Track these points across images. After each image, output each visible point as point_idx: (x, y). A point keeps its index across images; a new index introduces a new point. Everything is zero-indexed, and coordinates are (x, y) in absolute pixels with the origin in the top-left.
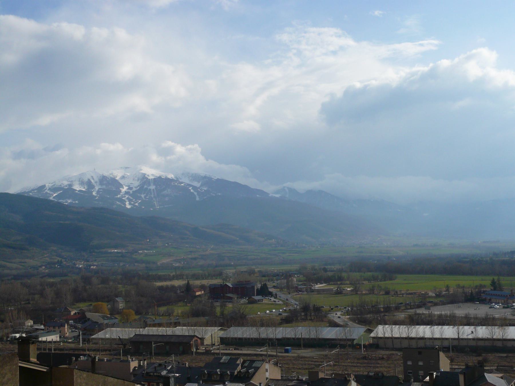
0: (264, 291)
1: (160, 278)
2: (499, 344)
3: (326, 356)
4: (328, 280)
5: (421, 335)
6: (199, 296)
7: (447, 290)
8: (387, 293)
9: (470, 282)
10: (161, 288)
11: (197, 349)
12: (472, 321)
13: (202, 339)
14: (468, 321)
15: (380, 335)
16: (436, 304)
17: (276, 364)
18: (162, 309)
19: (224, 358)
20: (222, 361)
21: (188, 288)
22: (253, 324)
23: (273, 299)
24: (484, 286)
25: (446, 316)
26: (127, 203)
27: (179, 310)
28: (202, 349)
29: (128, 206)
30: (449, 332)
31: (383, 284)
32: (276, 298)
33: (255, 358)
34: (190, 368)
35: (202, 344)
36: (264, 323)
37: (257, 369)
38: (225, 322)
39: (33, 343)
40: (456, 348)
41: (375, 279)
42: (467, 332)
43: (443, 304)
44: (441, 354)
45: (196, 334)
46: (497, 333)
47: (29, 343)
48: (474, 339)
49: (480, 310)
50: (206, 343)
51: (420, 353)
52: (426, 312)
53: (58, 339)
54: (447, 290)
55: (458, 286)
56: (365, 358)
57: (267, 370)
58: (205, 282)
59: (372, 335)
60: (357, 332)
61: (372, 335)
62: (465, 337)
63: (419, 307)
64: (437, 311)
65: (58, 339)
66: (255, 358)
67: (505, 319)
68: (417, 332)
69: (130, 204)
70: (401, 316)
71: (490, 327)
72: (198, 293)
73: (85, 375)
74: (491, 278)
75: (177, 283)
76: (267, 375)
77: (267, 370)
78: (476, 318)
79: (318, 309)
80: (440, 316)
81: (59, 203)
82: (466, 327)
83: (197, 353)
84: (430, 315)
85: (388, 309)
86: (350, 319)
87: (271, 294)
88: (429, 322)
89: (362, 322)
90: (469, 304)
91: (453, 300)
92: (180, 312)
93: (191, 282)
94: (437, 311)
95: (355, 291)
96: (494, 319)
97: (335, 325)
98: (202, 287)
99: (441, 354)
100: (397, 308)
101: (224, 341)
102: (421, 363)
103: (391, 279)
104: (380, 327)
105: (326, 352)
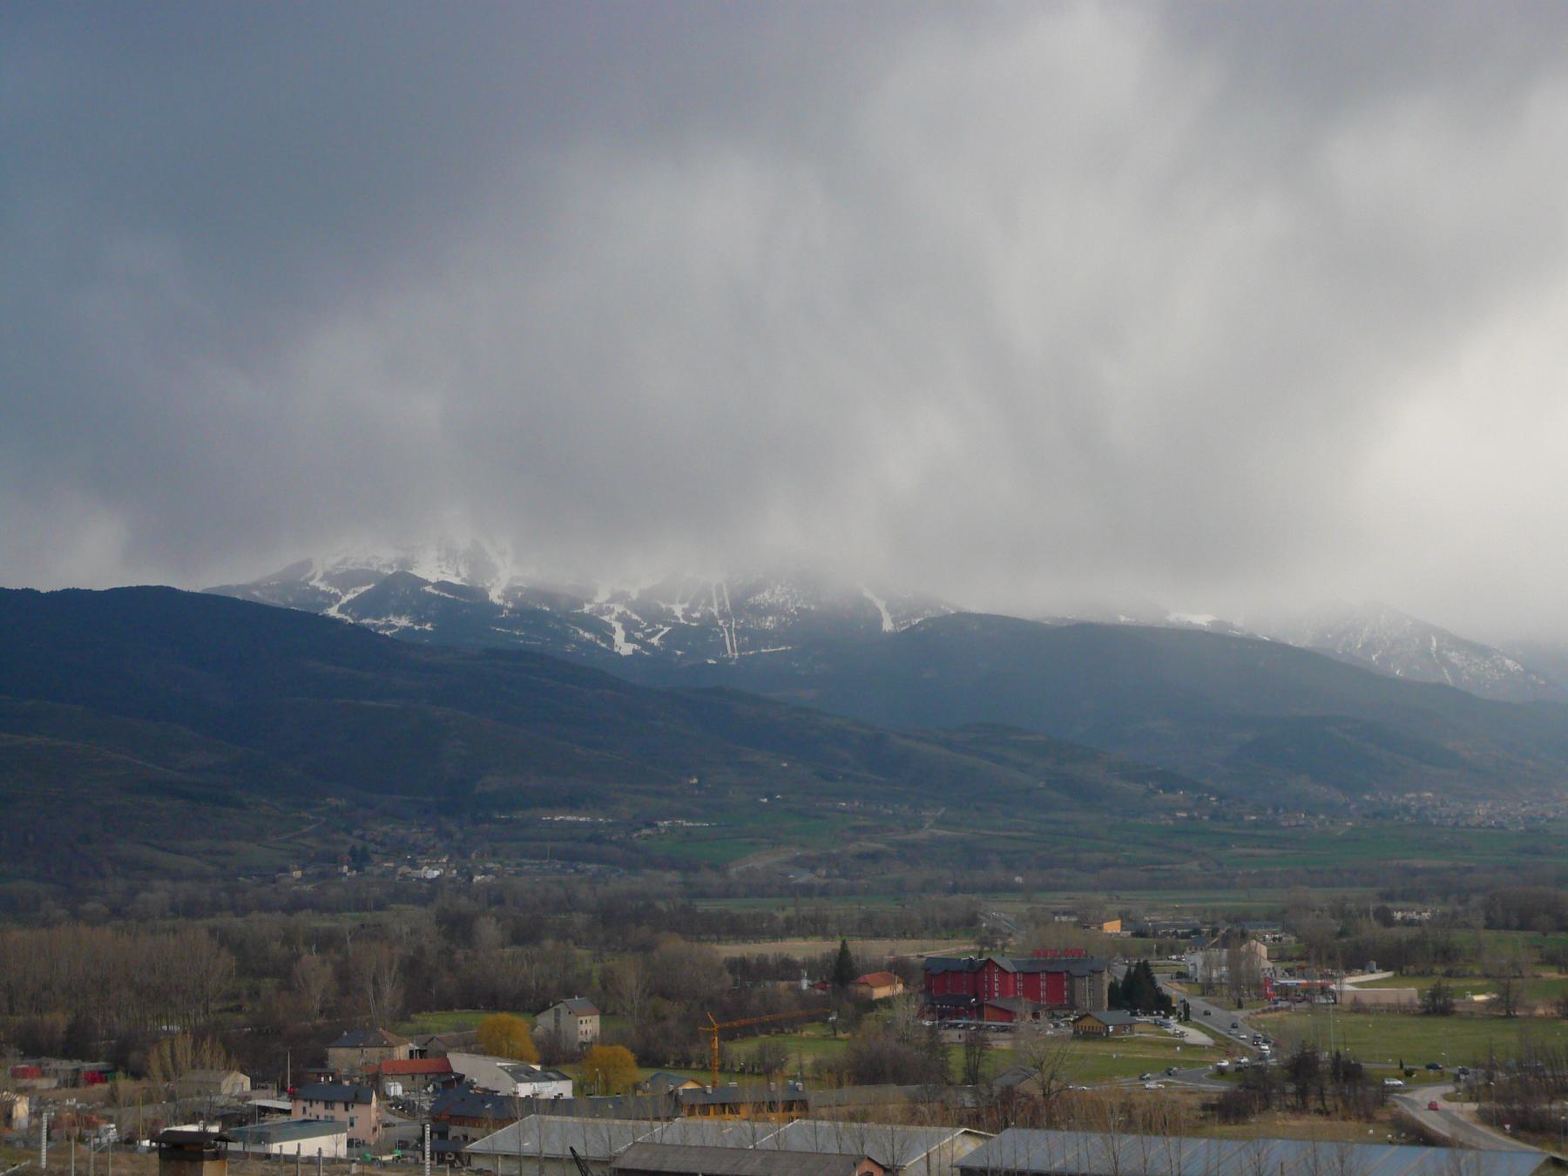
0: (1137, 994)
1: (737, 929)
4: (1396, 960)
6: (887, 1002)
10: (740, 967)
18: (742, 1050)
21: (842, 972)
22: (1091, 1117)
23: (1174, 1026)
26: (619, 636)
27: (805, 1051)
29: (625, 649)
32: (1185, 1018)
45: (869, 1150)
65: (342, 1151)
69: (629, 638)
72: (880, 993)
75: (800, 948)
79: (1348, 1072)
81: (365, 630)
86: (1486, 1118)
87: (1163, 1004)
92: (808, 1060)
93: (857, 946)
95: (1505, 1008)
98: (900, 969)
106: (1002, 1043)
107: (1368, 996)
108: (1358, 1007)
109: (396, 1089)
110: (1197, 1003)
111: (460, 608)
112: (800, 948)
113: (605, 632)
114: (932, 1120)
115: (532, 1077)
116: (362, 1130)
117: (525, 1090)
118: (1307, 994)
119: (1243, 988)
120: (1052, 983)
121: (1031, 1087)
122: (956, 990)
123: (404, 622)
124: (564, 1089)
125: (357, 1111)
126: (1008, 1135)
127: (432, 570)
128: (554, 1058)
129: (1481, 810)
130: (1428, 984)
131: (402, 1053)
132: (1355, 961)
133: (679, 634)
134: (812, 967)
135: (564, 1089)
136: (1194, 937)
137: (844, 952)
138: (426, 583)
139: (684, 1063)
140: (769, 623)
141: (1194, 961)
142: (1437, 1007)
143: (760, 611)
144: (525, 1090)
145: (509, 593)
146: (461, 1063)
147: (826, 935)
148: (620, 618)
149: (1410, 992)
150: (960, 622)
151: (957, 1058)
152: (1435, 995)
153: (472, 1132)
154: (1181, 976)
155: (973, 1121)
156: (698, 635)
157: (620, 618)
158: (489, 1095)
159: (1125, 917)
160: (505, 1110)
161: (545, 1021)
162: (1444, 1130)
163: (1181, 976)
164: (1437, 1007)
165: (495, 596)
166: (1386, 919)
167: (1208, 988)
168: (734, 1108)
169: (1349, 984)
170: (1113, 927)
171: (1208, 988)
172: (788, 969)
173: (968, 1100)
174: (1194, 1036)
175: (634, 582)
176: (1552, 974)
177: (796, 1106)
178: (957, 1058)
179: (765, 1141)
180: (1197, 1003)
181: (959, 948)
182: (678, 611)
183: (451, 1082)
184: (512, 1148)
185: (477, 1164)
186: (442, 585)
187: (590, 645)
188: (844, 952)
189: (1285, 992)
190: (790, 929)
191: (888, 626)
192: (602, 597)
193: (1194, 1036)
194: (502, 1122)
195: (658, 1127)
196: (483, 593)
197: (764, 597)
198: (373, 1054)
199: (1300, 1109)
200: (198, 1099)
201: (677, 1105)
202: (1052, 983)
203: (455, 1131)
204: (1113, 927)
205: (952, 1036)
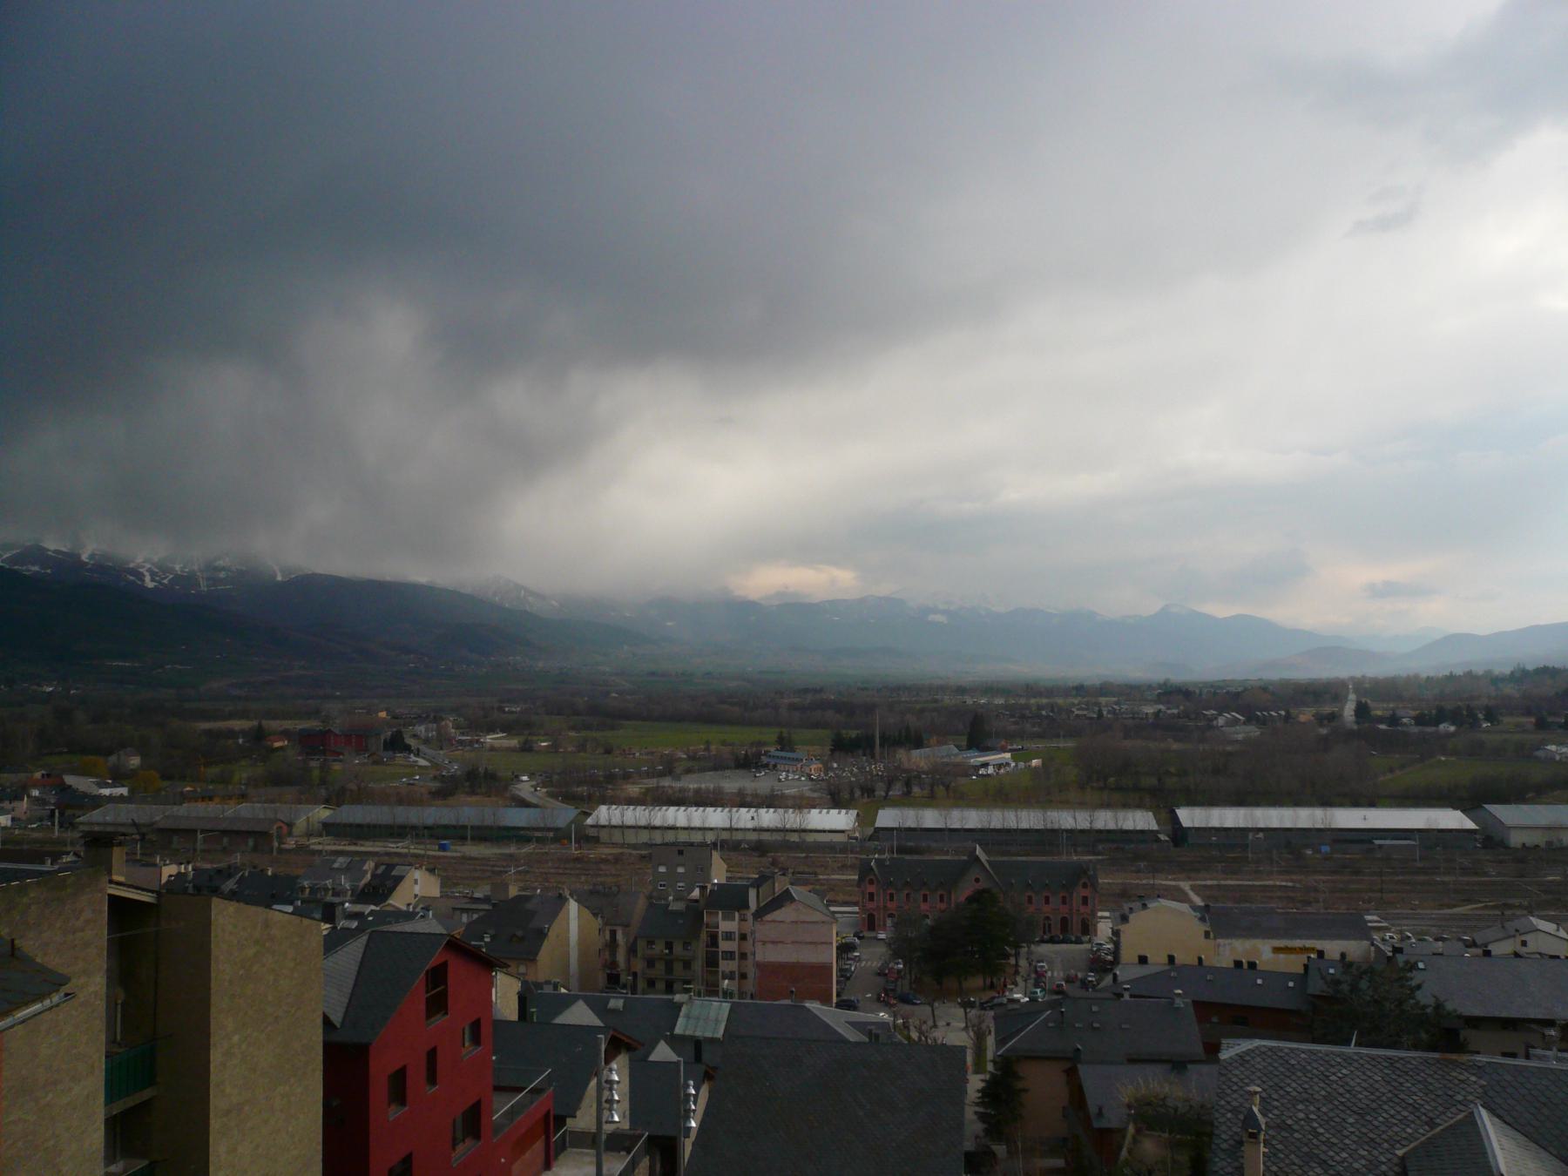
0: (396, 744)
1: (205, 715)
2: (794, 838)
3: (511, 855)
4: (508, 728)
5: (670, 822)
6: (281, 748)
7: (707, 749)
8: (608, 751)
9: (741, 737)
10: (209, 732)
11: (280, 843)
12: (748, 799)
13: (290, 825)
14: (742, 800)
15: (603, 822)
16: (689, 771)
17: (431, 871)
18: (214, 771)
19: (341, 859)
20: (336, 865)
21: (259, 735)
22: (383, 798)
23: (413, 758)
24: (765, 744)
25: (708, 791)
26: (148, 578)
27: (243, 772)
28: (291, 843)
29: (150, 585)
30: (715, 817)
31: (598, 734)
32: (417, 755)
33: (396, 860)
34: (275, 876)
35: (290, 834)
36: (405, 799)
37: (400, 879)
38: (335, 798)
39: (120, 844)
40: (729, 843)
41: (588, 727)
42: (744, 817)
43: (702, 770)
44: (716, 855)
45: (280, 816)
46: (792, 819)
47: (112, 845)
48: (754, 830)
49: (732, 783)
50: (296, 831)
51: (681, 853)
52: (678, 785)
53: (9, 823)
54: (707, 749)
55: (724, 743)
56: (577, 860)
57: (416, 882)
58: (288, 724)
59: (589, 821)
60: (564, 815)
61: (589, 821)
62: (741, 825)
63: (662, 775)
64: (691, 783)
65: (9, 823)
66: (396, 860)
67: (802, 797)
68: (664, 817)
69: (153, 580)
70: (634, 790)
71: (781, 811)
72: (277, 745)
73: (231, 909)
74: (777, 730)
75: (237, 724)
76: (417, 890)
77: (416, 882)
78: (756, 795)
79: (491, 777)
80: (698, 791)
81: (16, 572)
82: (743, 810)
83: (280, 851)
84: (682, 790)
85: (611, 778)
86: (550, 794)
87: (408, 749)
88: (679, 801)
89: (569, 798)
90: (741, 772)
91: (718, 766)
92: (244, 775)
93: (264, 723)
94: (691, 783)
95: (554, 748)
96: (783, 796)
97: (524, 804)
98: (286, 734)
99: (716, 855)
100: (627, 777)
101: (329, 828)
102: (681, 870)
103: (612, 728)
104: (603, 809)
105: (512, 849)
106: (337, 767)
107: (497, 744)
108: (492, 749)
109: (36, 793)
110: (422, 747)
111: (68, 564)
112: (237, 724)
113: (140, 576)
114: (308, 802)
115: (107, 786)
116: (17, 814)
117: (106, 792)
118: (471, 743)
119: (443, 741)
120: (359, 739)
121: (353, 786)
122: (314, 743)
123: (36, 568)
124: (124, 791)
125: (16, 804)
126: (345, 808)
127: (52, 544)
128: (118, 777)
129: (541, 664)
130: (522, 739)
131: (38, 775)
132: (491, 730)
133: (178, 579)
134: (243, 733)
135: (124, 791)
136: (420, 719)
137: (260, 726)
138: (1195, 908)
139: (183, 778)
140: (222, 575)
141: (421, 729)
142: (526, 748)
143: (218, 569)
144: (106, 792)
145: (92, 556)
146: (69, 780)
147: (248, 718)
148: (149, 570)
149: (514, 742)
150: (314, 574)
151: (316, 773)
152: (526, 742)
153: (77, 812)
154: (415, 736)
155: (327, 801)
156: (188, 580)
157: (149, 570)
158: (85, 795)
159: (387, 710)
160: (97, 802)
161: (113, 759)
162: (534, 800)
163: (415, 736)
164: (526, 748)
165: (84, 558)
166: (501, 709)
167: (427, 741)
168: (211, 799)
169: (489, 739)
170: (383, 714)
171: (427, 741)
172: (232, 734)
173: (323, 792)
174: (422, 762)
175: (148, 553)
176: (572, 734)
177: (243, 797)
178: (316, 773)
179: (229, 813)
180: (422, 747)
181: (312, 724)
182: (177, 567)
183: (65, 789)
184: (101, 820)
185: (82, 828)
186: (55, 551)
187: (133, 583)
188: (260, 726)
189: (461, 742)
190: (231, 716)
191: (279, 578)
192: (139, 560)
193: (422, 762)
194: (98, 806)
195: (175, 808)
196: (79, 556)
197: (221, 563)
198: (22, 776)
199: (473, 793)
200: (1389, 776)
201: (184, 798)
202: (359, 739)
203: (69, 812)
204: (383, 714)
205: (313, 764)
